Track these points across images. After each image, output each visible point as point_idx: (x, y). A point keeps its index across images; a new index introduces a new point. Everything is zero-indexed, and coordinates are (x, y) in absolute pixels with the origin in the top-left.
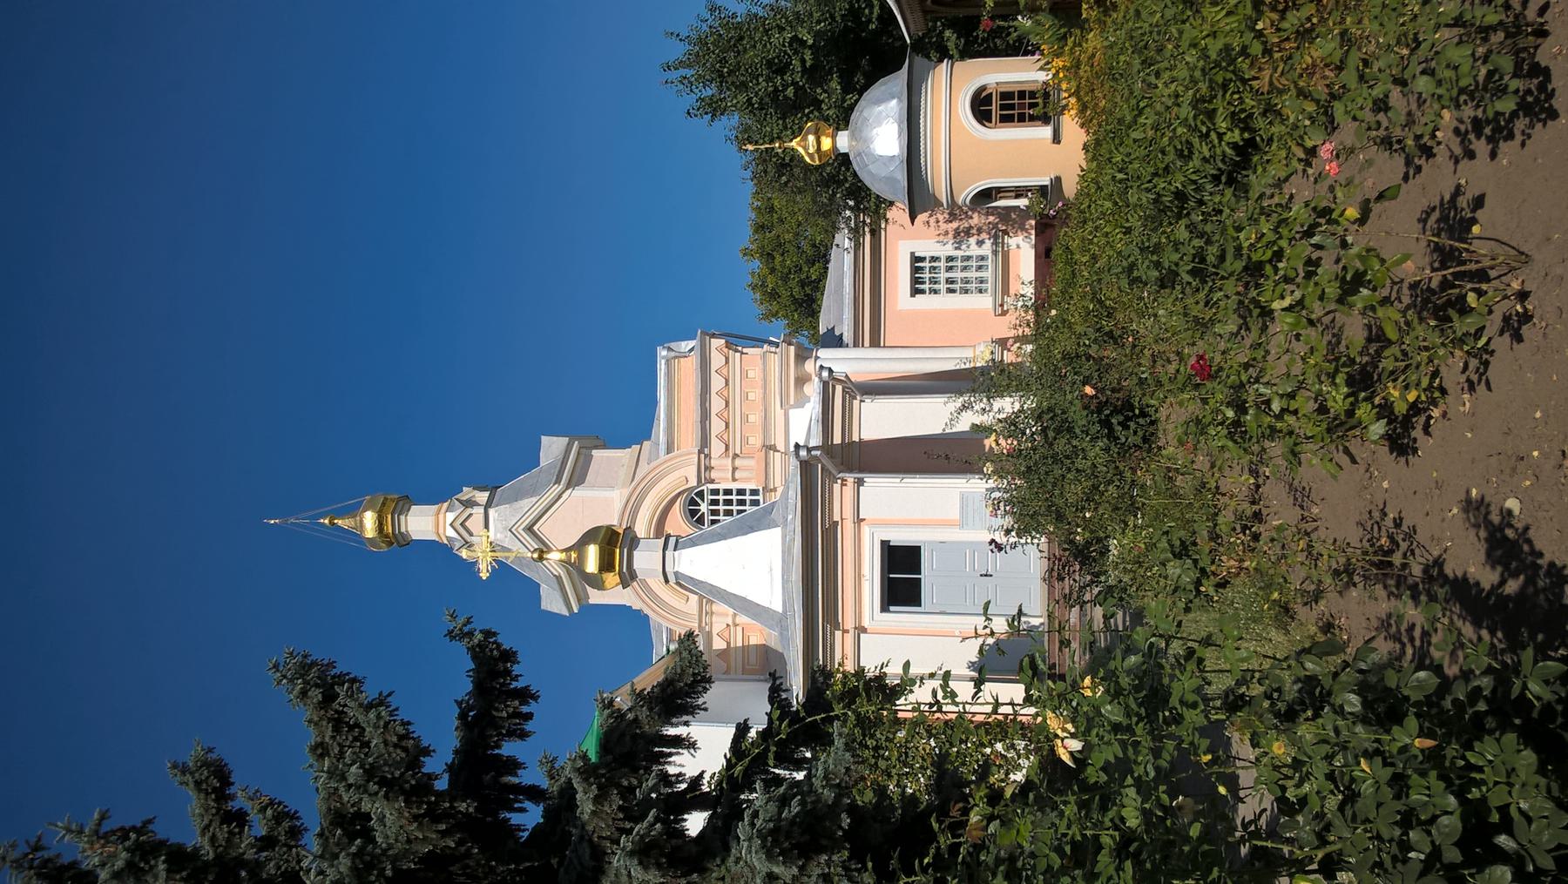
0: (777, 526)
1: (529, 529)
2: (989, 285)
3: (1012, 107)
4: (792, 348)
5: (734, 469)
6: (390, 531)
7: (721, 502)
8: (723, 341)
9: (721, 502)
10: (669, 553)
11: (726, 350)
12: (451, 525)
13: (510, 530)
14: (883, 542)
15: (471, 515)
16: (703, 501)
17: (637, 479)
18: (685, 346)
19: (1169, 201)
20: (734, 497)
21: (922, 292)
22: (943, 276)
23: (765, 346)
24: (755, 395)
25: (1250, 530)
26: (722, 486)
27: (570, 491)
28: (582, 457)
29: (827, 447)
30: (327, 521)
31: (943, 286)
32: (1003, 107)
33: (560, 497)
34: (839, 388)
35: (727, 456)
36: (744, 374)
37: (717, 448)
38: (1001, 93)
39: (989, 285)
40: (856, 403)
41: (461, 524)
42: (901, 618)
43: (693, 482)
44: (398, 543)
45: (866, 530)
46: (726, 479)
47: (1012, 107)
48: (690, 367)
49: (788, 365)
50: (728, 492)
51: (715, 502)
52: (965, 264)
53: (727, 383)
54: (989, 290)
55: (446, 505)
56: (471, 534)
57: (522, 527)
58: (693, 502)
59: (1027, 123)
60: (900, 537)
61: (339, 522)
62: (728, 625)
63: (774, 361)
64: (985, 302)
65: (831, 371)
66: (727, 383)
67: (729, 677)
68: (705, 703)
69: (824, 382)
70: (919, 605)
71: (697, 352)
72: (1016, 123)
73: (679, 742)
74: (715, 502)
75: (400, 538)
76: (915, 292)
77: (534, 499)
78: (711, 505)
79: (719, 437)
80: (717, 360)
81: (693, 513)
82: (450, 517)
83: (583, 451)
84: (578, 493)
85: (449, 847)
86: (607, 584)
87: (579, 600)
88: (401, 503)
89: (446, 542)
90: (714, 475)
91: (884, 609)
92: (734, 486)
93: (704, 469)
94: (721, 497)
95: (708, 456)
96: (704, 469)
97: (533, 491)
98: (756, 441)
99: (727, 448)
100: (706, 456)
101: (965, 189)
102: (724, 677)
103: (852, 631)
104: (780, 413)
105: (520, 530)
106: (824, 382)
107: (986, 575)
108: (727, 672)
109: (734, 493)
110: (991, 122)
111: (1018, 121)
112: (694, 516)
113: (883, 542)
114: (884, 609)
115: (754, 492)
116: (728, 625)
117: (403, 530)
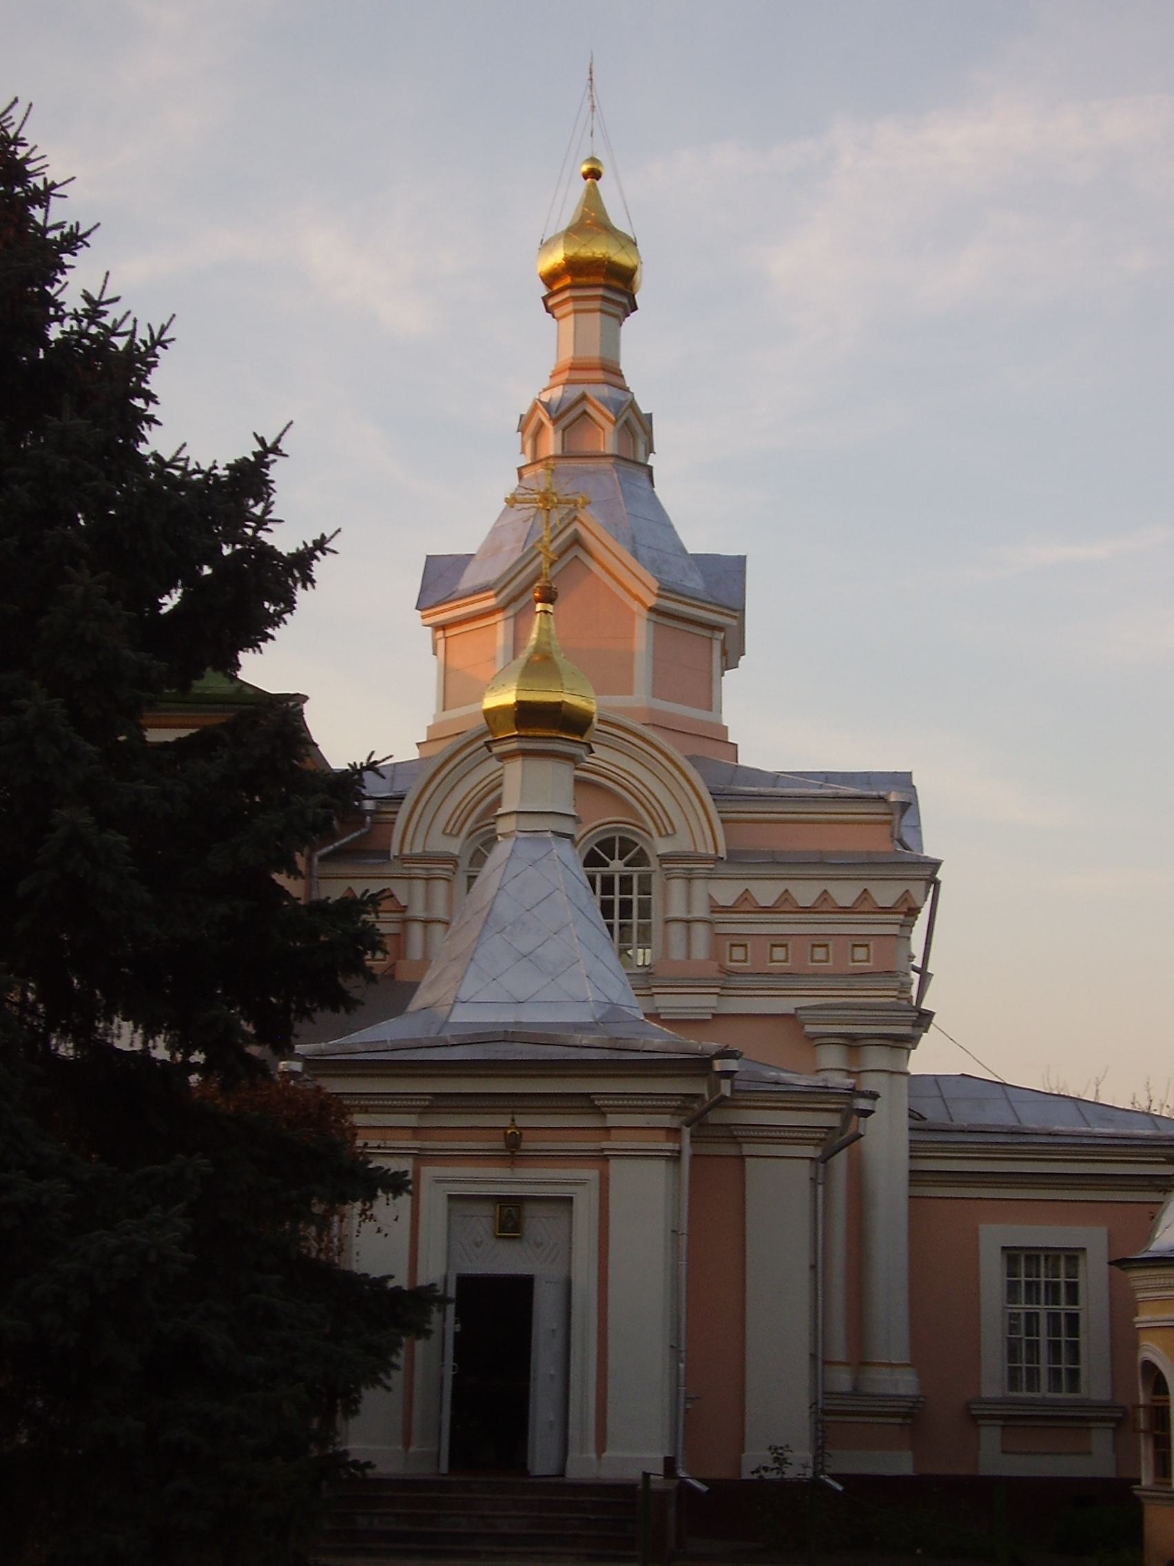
2: (1024, 1394)
5: (427, 922)
16: (626, 865)
27: (645, 613)
31: (1022, 1307)
40: (810, 1151)
45: (591, 1174)
50: (645, 911)
51: (626, 881)
58: (627, 845)
76: (1011, 1255)
78: (621, 878)
79: (746, 896)
105: (575, 525)
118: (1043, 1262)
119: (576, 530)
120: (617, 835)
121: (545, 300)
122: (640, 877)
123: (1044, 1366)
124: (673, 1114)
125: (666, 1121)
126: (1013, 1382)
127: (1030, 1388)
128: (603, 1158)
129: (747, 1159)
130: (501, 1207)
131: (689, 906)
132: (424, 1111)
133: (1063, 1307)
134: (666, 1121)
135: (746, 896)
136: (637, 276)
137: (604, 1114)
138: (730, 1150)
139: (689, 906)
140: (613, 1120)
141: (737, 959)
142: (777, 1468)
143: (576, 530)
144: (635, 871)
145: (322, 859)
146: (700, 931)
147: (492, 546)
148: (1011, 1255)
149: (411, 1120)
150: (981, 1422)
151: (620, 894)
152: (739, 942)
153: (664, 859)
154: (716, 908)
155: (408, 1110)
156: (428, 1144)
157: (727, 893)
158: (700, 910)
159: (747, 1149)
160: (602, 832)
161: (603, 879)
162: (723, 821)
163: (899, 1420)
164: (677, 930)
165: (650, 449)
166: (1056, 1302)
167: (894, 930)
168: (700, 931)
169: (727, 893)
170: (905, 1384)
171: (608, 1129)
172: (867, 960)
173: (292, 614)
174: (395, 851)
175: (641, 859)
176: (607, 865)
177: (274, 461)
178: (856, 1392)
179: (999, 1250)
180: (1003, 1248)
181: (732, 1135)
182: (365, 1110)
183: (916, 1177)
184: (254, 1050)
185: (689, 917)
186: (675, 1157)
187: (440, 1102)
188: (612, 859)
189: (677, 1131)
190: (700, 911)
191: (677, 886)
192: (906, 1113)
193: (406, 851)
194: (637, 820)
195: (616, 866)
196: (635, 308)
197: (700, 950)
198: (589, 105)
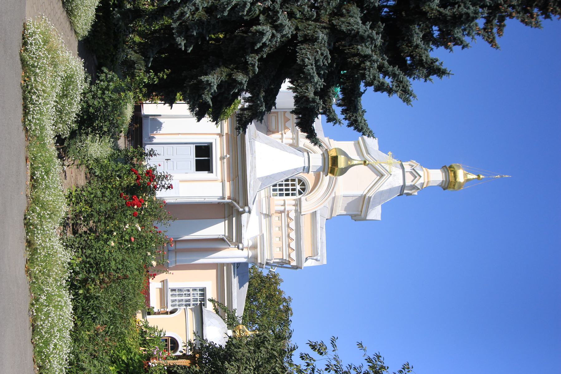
0: (259, 178)
1: (382, 175)
4: (259, 261)
5: (284, 205)
7: (290, 190)
8: (292, 264)
9: (290, 190)
10: (307, 165)
11: (290, 260)
12: (420, 176)
13: (391, 174)
14: (212, 172)
15: (412, 182)
16: (299, 190)
17: (331, 198)
18: (310, 263)
19: (183, 14)
20: (284, 192)
21: (200, 290)
23: (272, 262)
24: (276, 240)
26: (290, 197)
27: (365, 193)
28: (360, 210)
29: (239, 214)
30: (481, 177)
33: (369, 191)
34: (234, 241)
35: (288, 211)
36: (281, 249)
37: (292, 215)
41: (416, 177)
42: (203, 140)
44: (446, 167)
45: (219, 177)
46: (288, 200)
48: (306, 251)
49: (261, 253)
50: (287, 195)
52: (181, 303)
54: (170, 295)
55: (425, 186)
57: (385, 177)
58: (304, 190)
60: (204, 174)
61: (475, 177)
62: (285, 134)
63: (267, 256)
64: (171, 285)
65: (238, 248)
67: (285, 110)
69: (241, 243)
70: (211, 144)
71: (304, 259)
75: (446, 170)
77: (381, 189)
79: (291, 219)
80: (293, 255)
81: (303, 184)
82: (421, 180)
83: (359, 213)
84: (359, 192)
85: (300, 80)
86: (334, 150)
87: (359, 143)
88: (446, 186)
89: (424, 169)
90: (294, 202)
92: (285, 197)
94: (284, 192)
95: (296, 211)
96: (298, 204)
97: (382, 193)
98: (275, 218)
99: (288, 214)
100: (297, 210)
102: (286, 110)
103: (224, 134)
104: (264, 231)
105: (386, 175)
106: (241, 243)
107: (168, 160)
108: (285, 112)
109: (284, 194)
112: (302, 183)
113: (212, 172)
114: (211, 144)
116: (285, 134)
117: (444, 174)
118: (203, 297)
119: (385, 175)
122: (295, 193)
123: (177, 298)
126: (173, 290)
130: (360, 215)
138: (226, 215)
142: (82, 250)
143: (385, 175)
144: (297, 192)
151: (196, 157)
153: (300, 199)
158: (288, 208)
160: (306, 183)
173: (214, 309)
175: (300, 193)
176: (298, 185)
177: (398, 95)
184: (226, 14)
185: (286, 206)
194: (372, 205)
195: (298, 187)
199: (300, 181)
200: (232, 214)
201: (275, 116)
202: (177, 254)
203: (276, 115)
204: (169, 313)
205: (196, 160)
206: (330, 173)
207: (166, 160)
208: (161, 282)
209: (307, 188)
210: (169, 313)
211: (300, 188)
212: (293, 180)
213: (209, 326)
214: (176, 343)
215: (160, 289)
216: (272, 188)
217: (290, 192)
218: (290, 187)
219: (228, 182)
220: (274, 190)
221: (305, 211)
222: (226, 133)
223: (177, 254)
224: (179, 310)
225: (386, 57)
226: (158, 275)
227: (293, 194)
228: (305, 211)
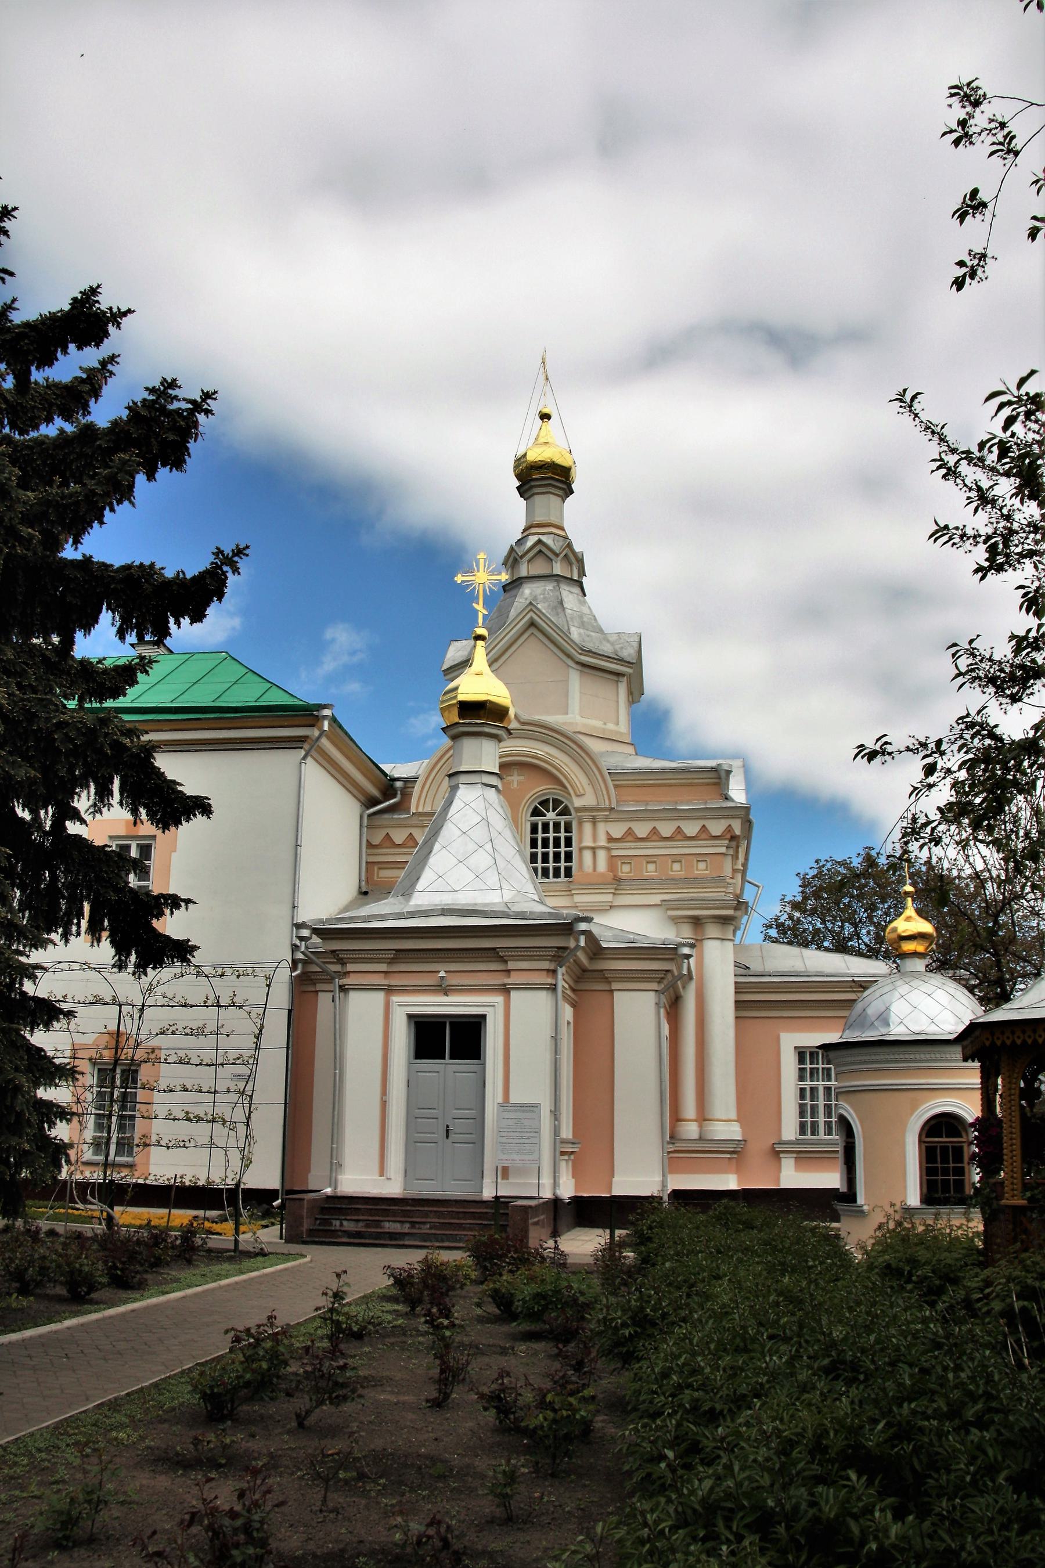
2: (809, 1137)
3: (944, 1160)
5: (593, 849)
6: (534, 477)
22: (821, 1084)
25: (570, 1458)
31: (808, 1084)
32: (944, 1149)
38: (961, 1148)
39: (809, 1137)
40: (655, 986)
43: (578, 803)
45: (498, 999)
47: (944, 1160)
49: (678, 909)
50: (569, 842)
51: (557, 826)
53: (642, 839)
56: (529, 561)
58: (557, 803)
59: (925, 1178)
64: (789, 1131)
66: (642, 839)
68: (142, 823)
72: (924, 1165)
73: (103, 794)
74: (557, 826)
76: (801, 1054)
78: (554, 824)
79: (630, 832)
81: (544, 803)
91: (410, 1017)
92: (574, 849)
93: (594, 815)
101: (855, 1112)
104: (656, 899)
107: (447, 1131)
110: (927, 1136)
111: (963, 1175)
114: (410, 1017)
115: (568, 873)
117: (536, 490)
119: (531, 618)
120: (551, 797)
121: (518, 488)
124: (551, 961)
125: (546, 965)
127: (813, 1134)
128: (505, 990)
129: (615, 993)
131: (595, 838)
132: (391, 961)
133: (808, 1084)
134: (552, 966)
135: (630, 832)
136: (572, 472)
137: (506, 962)
139: (595, 838)
140: (511, 965)
141: (624, 871)
143: (531, 618)
144: (562, 820)
145: (369, 816)
146: (602, 855)
147: (591, 624)
148: (801, 1054)
149: (383, 967)
150: (782, 1155)
152: (626, 859)
153: (578, 810)
154: (611, 839)
155: (379, 961)
156: (393, 983)
157: (618, 830)
159: (614, 986)
161: (566, 823)
162: (616, 786)
163: (728, 1156)
164: (587, 855)
165: (582, 573)
166: (829, 1080)
167: (723, 850)
168: (602, 855)
169: (618, 830)
170: (733, 1131)
171: (509, 971)
172: (706, 869)
174: (413, 810)
175: (565, 812)
176: (545, 815)
178: (701, 1139)
179: (793, 1049)
180: (796, 1048)
181: (603, 976)
182: (356, 961)
183: (739, 1005)
186: (553, 988)
187: (400, 955)
188: (548, 811)
189: (554, 972)
190: (602, 841)
191: (588, 827)
192: (732, 964)
193: (420, 810)
195: (551, 816)
196: (572, 492)
197: (602, 865)
198: (542, 377)
199: (536, 812)
200: (602, 971)
201: (380, 868)
202: (707, 1117)
203: (376, 868)
204: (850, 1140)
205: (451, 1058)
206: (855, 1201)
207: (447, 1137)
208: (780, 1159)
209: (555, 794)
210: (850, 1140)
211: (554, 811)
212: (534, 829)
213: (889, 1025)
214: (933, 1122)
215: (679, 1120)
216: (551, 879)
217: (562, 835)
218: (551, 835)
219: (509, 977)
220: (557, 874)
221: (609, 799)
222: (385, 978)
223: (710, 1117)
224: (842, 1111)
225: (69, 428)
226: (906, 1196)
227: (568, 829)
228: (609, 799)
